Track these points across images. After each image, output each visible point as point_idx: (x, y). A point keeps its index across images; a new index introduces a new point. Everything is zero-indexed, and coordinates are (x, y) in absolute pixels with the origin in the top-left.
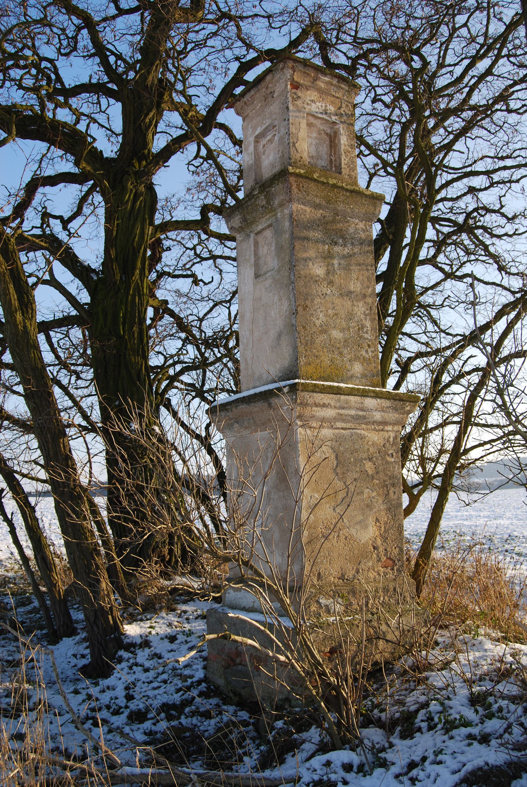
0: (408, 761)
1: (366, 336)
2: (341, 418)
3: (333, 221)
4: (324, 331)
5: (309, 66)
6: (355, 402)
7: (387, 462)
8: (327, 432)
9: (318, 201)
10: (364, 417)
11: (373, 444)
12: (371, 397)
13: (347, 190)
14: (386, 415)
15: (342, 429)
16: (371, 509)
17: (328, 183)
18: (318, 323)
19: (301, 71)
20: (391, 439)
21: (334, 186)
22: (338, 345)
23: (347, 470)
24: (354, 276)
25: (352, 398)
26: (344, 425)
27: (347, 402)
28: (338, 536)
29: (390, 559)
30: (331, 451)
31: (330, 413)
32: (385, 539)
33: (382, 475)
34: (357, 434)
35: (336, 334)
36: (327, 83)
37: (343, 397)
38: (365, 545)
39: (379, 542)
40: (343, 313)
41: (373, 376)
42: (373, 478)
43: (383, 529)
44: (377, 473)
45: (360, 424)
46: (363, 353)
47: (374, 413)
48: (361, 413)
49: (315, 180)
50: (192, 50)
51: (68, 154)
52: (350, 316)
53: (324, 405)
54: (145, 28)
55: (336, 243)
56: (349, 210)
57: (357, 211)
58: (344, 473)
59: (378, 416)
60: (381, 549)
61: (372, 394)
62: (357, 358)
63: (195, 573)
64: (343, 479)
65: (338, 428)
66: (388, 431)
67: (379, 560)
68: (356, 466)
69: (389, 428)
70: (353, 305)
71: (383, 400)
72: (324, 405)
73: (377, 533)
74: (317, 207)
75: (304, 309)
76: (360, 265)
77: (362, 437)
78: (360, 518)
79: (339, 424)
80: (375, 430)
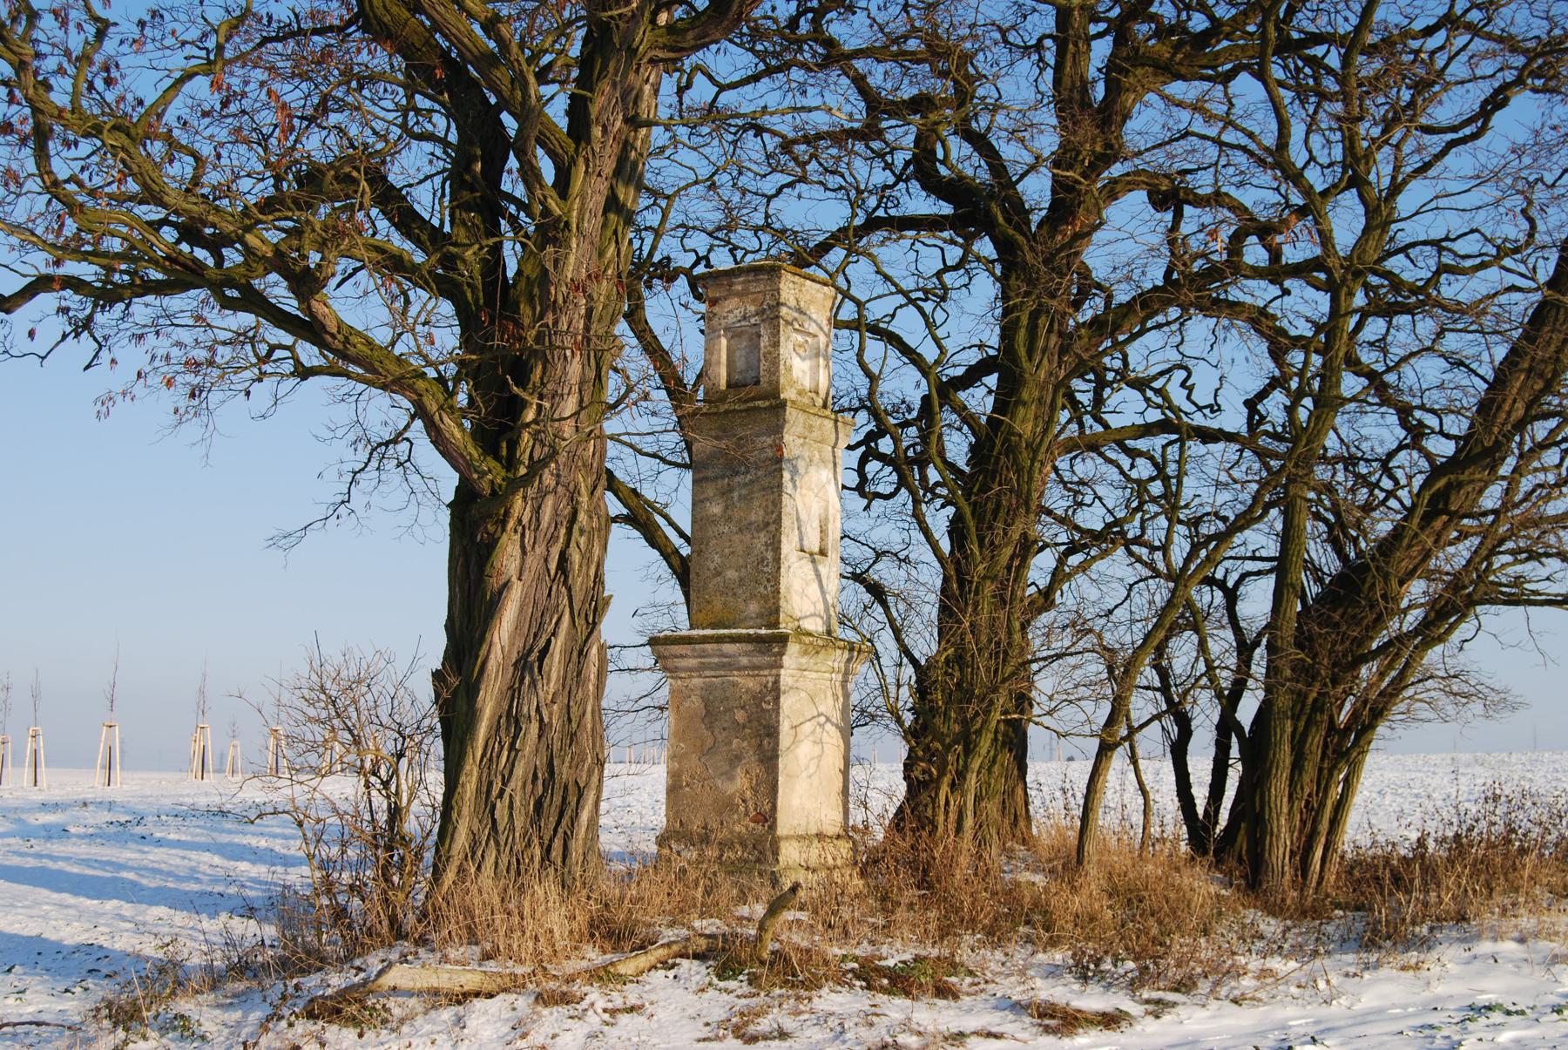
0: (296, 667)
4: (718, 574)
7: (763, 710)
10: (730, 664)
18: (712, 566)
21: (727, 412)
24: (756, 503)
25: (708, 646)
31: (693, 662)
32: (755, 791)
33: (755, 724)
35: (731, 574)
38: (731, 797)
39: (748, 794)
40: (740, 549)
50: (738, 116)
52: (748, 550)
53: (682, 656)
54: (125, 875)
55: (737, 473)
59: (744, 661)
60: (750, 804)
62: (753, 596)
64: (710, 728)
67: (747, 814)
69: (766, 672)
72: (682, 656)
77: (734, 685)
79: (708, 673)
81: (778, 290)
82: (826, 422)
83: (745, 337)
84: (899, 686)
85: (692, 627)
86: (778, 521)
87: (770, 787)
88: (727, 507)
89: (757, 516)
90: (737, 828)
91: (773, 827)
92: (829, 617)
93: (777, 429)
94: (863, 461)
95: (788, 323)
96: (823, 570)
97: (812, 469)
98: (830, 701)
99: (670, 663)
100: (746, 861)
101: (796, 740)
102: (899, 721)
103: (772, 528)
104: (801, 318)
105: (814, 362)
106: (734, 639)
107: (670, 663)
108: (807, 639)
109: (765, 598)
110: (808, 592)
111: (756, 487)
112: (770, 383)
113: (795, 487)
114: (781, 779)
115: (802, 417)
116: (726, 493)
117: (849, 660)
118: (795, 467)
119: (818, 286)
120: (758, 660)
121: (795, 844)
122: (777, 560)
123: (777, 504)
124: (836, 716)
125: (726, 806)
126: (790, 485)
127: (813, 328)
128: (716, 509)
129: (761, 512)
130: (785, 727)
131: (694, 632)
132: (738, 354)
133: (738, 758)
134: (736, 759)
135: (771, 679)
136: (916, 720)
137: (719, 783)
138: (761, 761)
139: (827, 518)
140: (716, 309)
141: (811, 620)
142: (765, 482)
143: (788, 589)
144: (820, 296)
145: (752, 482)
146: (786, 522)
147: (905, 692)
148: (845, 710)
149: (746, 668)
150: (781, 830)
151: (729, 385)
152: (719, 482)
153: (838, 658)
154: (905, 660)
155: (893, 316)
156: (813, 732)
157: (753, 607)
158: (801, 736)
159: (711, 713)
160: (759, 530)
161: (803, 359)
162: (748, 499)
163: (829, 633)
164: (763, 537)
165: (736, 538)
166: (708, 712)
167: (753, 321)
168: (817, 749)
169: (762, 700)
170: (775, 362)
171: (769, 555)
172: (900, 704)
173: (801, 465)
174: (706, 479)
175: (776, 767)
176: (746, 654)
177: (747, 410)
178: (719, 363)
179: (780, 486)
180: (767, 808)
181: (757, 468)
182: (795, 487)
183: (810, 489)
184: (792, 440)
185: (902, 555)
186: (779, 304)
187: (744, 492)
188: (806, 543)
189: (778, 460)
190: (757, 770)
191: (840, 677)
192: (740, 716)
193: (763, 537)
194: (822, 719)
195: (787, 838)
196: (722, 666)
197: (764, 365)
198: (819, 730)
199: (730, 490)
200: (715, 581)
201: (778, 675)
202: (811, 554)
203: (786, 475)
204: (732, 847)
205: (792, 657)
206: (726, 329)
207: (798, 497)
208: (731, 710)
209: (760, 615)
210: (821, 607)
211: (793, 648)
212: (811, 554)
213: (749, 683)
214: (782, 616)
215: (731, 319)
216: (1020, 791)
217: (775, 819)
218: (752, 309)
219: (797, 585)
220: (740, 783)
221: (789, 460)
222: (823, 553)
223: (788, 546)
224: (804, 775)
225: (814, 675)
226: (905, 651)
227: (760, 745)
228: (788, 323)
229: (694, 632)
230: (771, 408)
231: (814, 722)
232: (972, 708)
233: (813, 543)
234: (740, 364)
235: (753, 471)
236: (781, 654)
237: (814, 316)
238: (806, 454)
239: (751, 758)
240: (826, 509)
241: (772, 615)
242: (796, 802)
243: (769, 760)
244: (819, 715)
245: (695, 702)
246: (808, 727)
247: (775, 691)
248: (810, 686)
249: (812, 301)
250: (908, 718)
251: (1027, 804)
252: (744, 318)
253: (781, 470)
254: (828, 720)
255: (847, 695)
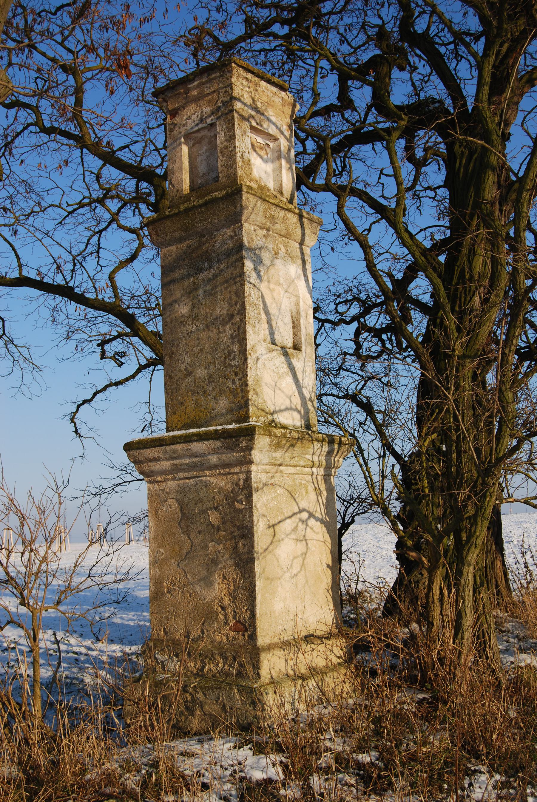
1: (233, 363)
2: (176, 469)
3: (199, 246)
4: (189, 374)
5: (176, 86)
6: (182, 450)
7: (236, 510)
8: (172, 484)
9: (177, 235)
11: (219, 492)
12: (196, 441)
13: (200, 206)
14: (224, 457)
15: (187, 478)
16: (216, 565)
17: (180, 212)
18: (183, 367)
19: (171, 97)
20: (241, 482)
21: (187, 210)
22: (203, 384)
23: (192, 523)
24: (220, 297)
25: (178, 447)
26: (186, 475)
27: (174, 452)
28: (183, 592)
29: (239, 622)
30: (176, 503)
31: (166, 465)
32: (233, 597)
34: (201, 482)
36: (198, 86)
37: (168, 448)
38: (210, 604)
41: (240, 409)
42: (219, 529)
43: (232, 588)
44: (224, 523)
45: (203, 470)
46: (230, 384)
47: (210, 457)
48: (195, 460)
49: (168, 217)
51: (63, 283)
55: (201, 270)
56: (209, 226)
57: (216, 221)
58: (188, 526)
59: (214, 459)
60: (229, 611)
61: (196, 438)
62: (222, 392)
63: (497, 617)
64: (187, 532)
65: (182, 479)
66: (237, 473)
67: (226, 623)
68: (200, 518)
69: (236, 470)
70: (220, 332)
71: (211, 442)
72: (155, 460)
73: (225, 591)
74: (181, 240)
75: (171, 357)
76: (226, 281)
77: (207, 485)
78: (204, 574)
79: (181, 475)
80: (220, 474)
81: (231, 85)
82: (290, 215)
83: (205, 141)
84: (384, 477)
85: (168, 430)
86: (242, 311)
87: (247, 593)
88: (193, 306)
89: (222, 309)
90: (218, 638)
91: (253, 637)
92: (307, 412)
93: (235, 219)
94: (357, 333)
95: (243, 118)
96: (298, 364)
97: (279, 262)
98: (313, 496)
99: (146, 468)
100: (227, 674)
101: (274, 539)
102: (386, 512)
103: (237, 319)
104: (257, 116)
105: (276, 164)
106: (201, 437)
107: (146, 468)
108: (278, 432)
109: (233, 392)
110: (278, 386)
111: (220, 280)
112: (228, 176)
113: (259, 277)
114: (259, 584)
115: (261, 206)
116: (191, 292)
117: (330, 453)
118: (258, 257)
119: (274, 89)
120: (228, 457)
121: (279, 653)
122: (244, 352)
123: (240, 294)
124: (320, 511)
125: (207, 614)
126: (253, 275)
127: (272, 130)
128: (183, 310)
129: (226, 306)
130: (260, 528)
131: (172, 434)
132: (199, 159)
133: (215, 562)
134: (213, 563)
135: (242, 476)
136: (403, 509)
137: (198, 589)
138: (237, 565)
139: (298, 313)
140: (177, 120)
141: (286, 414)
142: (227, 274)
143: (257, 381)
144: (278, 100)
145: (215, 276)
146: (250, 312)
147: (389, 484)
148: (329, 504)
149: (216, 467)
150: (262, 641)
151: (192, 188)
152: (186, 282)
153: (317, 452)
154: (387, 452)
155: (369, 230)
156: (295, 529)
157: (223, 403)
158: (280, 535)
159: (186, 517)
160: (224, 325)
161: (266, 161)
162: (211, 294)
163: (308, 426)
164: (229, 331)
165: (203, 335)
166: (183, 515)
167: (209, 121)
168: (301, 547)
169: (235, 499)
170: (231, 154)
171: (236, 348)
172: (386, 494)
173: (266, 257)
174: (173, 281)
175: (252, 571)
176: (215, 451)
177: (206, 204)
178: (181, 169)
179: (242, 274)
180: (246, 616)
181: (219, 261)
182: (259, 277)
183: (279, 284)
184: (251, 232)
185: (385, 380)
186: (232, 98)
187: (208, 288)
188: (277, 337)
189: (237, 250)
190: (233, 574)
191: (322, 471)
192: (214, 518)
193: (229, 331)
194: (305, 515)
195: (270, 648)
196: (193, 467)
197: (221, 161)
198: (301, 526)
199: (196, 287)
200: (186, 382)
201: (249, 472)
202: (283, 348)
203: (249, 265)
204: (212, 659)
205: (262, 451)
206: (188, 136)
207: (263, 286)
208: (204, 512)
209: (230, 411)
210: (297, 401)
211: (262, 442)
212: (283, 348)
213: (220, 482)
214: (251, 409)
215: (190, 124)
216: (498, 563)
217: (255, 628)
218: (208, 110)
219: (267, 377)
220: (218, 590)
221: (250, 249)
222: (296, 347)
223: (256, 336)
224: (287, 575)
225: (291, 470)
226: (388, 446)
227: (235, 548)
228: (243, 118)
229: (172, 434)
230: (228, 196)
231: (295, 519)
232: (463, 493)
233: (285, 337)
234: (202, 168)
235: (215, 266)
236: (250, 448)
237: (273, 119)
238: (271, 246)
239: (227, 561)
240: (297, 305)
241: (241, 408)
242: (278, 606)
243: (245, 562)
244: (300, 511)
245: (172, 506)
246: (288, 525)
247: (247, 489)
248: (288, 481)
249: (269, 104)
250: (396, 507)
251: (506, 574)
252: (201, 120)
253: (242, 258)
254: (311, 515)
255: (330, 489)
